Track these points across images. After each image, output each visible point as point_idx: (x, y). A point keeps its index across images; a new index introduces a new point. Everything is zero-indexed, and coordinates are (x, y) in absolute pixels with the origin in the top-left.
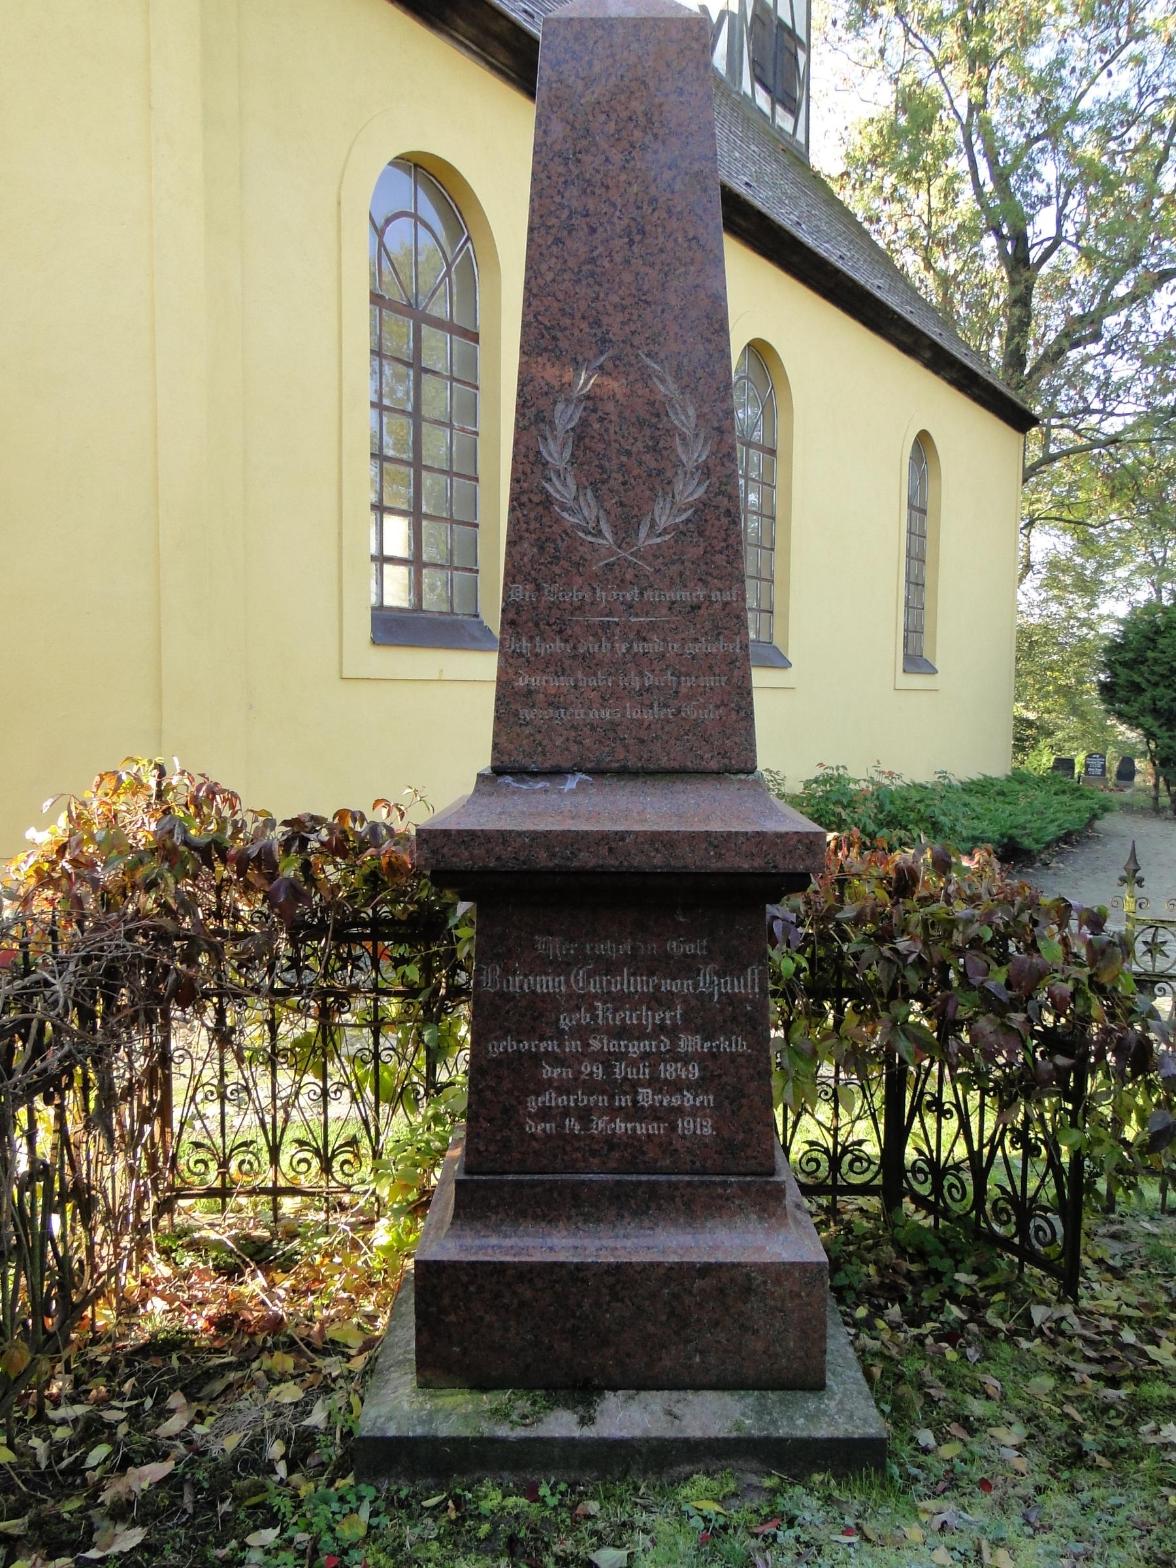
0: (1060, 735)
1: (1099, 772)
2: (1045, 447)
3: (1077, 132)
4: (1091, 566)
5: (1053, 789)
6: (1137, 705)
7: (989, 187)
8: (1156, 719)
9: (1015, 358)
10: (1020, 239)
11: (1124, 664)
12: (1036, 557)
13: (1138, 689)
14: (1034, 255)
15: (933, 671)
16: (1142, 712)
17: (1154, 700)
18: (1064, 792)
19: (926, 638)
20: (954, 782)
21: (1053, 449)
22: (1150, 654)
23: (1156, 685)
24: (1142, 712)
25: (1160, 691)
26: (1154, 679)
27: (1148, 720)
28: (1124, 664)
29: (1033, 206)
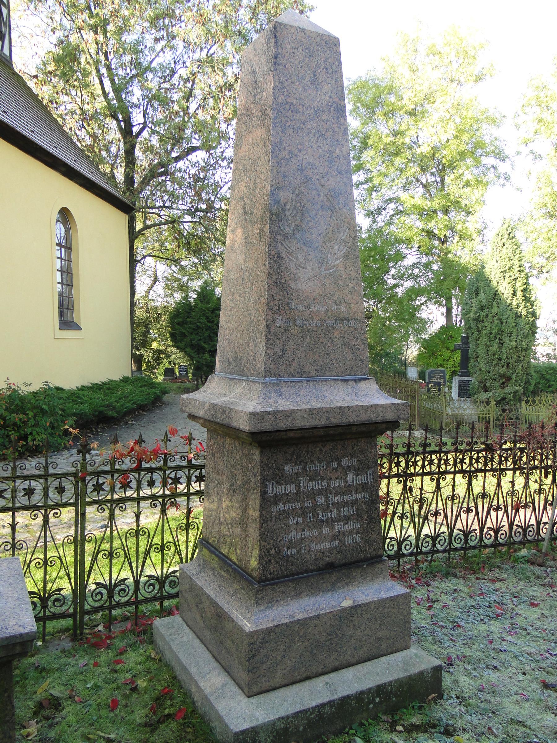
0: (173, 357)
1: (185, 373)
2: (145, 222)
3: (150, 76)
4: (185, 279)
5: (140, 385)
6: (183, 343)
7: (111, 95)
8: (192, 349)
9: (129, 180)
10: (128, 121)
11: (178, 324)
12: (159, 275)
13: (183, 335)
14: (135, 130)
15: (79, 328)
16: (186, 346)
17: (191, 340)
18: (145, 386)
19: (75, 311)
20: (51, 386)
21: (148, 223)
22: (188, 319)
23: (192, 333)
24: (186, 346)
25: (193, 336)
26: (191, 331)
27: (188, 350)
28: (178, 324)
29: (132, 107)
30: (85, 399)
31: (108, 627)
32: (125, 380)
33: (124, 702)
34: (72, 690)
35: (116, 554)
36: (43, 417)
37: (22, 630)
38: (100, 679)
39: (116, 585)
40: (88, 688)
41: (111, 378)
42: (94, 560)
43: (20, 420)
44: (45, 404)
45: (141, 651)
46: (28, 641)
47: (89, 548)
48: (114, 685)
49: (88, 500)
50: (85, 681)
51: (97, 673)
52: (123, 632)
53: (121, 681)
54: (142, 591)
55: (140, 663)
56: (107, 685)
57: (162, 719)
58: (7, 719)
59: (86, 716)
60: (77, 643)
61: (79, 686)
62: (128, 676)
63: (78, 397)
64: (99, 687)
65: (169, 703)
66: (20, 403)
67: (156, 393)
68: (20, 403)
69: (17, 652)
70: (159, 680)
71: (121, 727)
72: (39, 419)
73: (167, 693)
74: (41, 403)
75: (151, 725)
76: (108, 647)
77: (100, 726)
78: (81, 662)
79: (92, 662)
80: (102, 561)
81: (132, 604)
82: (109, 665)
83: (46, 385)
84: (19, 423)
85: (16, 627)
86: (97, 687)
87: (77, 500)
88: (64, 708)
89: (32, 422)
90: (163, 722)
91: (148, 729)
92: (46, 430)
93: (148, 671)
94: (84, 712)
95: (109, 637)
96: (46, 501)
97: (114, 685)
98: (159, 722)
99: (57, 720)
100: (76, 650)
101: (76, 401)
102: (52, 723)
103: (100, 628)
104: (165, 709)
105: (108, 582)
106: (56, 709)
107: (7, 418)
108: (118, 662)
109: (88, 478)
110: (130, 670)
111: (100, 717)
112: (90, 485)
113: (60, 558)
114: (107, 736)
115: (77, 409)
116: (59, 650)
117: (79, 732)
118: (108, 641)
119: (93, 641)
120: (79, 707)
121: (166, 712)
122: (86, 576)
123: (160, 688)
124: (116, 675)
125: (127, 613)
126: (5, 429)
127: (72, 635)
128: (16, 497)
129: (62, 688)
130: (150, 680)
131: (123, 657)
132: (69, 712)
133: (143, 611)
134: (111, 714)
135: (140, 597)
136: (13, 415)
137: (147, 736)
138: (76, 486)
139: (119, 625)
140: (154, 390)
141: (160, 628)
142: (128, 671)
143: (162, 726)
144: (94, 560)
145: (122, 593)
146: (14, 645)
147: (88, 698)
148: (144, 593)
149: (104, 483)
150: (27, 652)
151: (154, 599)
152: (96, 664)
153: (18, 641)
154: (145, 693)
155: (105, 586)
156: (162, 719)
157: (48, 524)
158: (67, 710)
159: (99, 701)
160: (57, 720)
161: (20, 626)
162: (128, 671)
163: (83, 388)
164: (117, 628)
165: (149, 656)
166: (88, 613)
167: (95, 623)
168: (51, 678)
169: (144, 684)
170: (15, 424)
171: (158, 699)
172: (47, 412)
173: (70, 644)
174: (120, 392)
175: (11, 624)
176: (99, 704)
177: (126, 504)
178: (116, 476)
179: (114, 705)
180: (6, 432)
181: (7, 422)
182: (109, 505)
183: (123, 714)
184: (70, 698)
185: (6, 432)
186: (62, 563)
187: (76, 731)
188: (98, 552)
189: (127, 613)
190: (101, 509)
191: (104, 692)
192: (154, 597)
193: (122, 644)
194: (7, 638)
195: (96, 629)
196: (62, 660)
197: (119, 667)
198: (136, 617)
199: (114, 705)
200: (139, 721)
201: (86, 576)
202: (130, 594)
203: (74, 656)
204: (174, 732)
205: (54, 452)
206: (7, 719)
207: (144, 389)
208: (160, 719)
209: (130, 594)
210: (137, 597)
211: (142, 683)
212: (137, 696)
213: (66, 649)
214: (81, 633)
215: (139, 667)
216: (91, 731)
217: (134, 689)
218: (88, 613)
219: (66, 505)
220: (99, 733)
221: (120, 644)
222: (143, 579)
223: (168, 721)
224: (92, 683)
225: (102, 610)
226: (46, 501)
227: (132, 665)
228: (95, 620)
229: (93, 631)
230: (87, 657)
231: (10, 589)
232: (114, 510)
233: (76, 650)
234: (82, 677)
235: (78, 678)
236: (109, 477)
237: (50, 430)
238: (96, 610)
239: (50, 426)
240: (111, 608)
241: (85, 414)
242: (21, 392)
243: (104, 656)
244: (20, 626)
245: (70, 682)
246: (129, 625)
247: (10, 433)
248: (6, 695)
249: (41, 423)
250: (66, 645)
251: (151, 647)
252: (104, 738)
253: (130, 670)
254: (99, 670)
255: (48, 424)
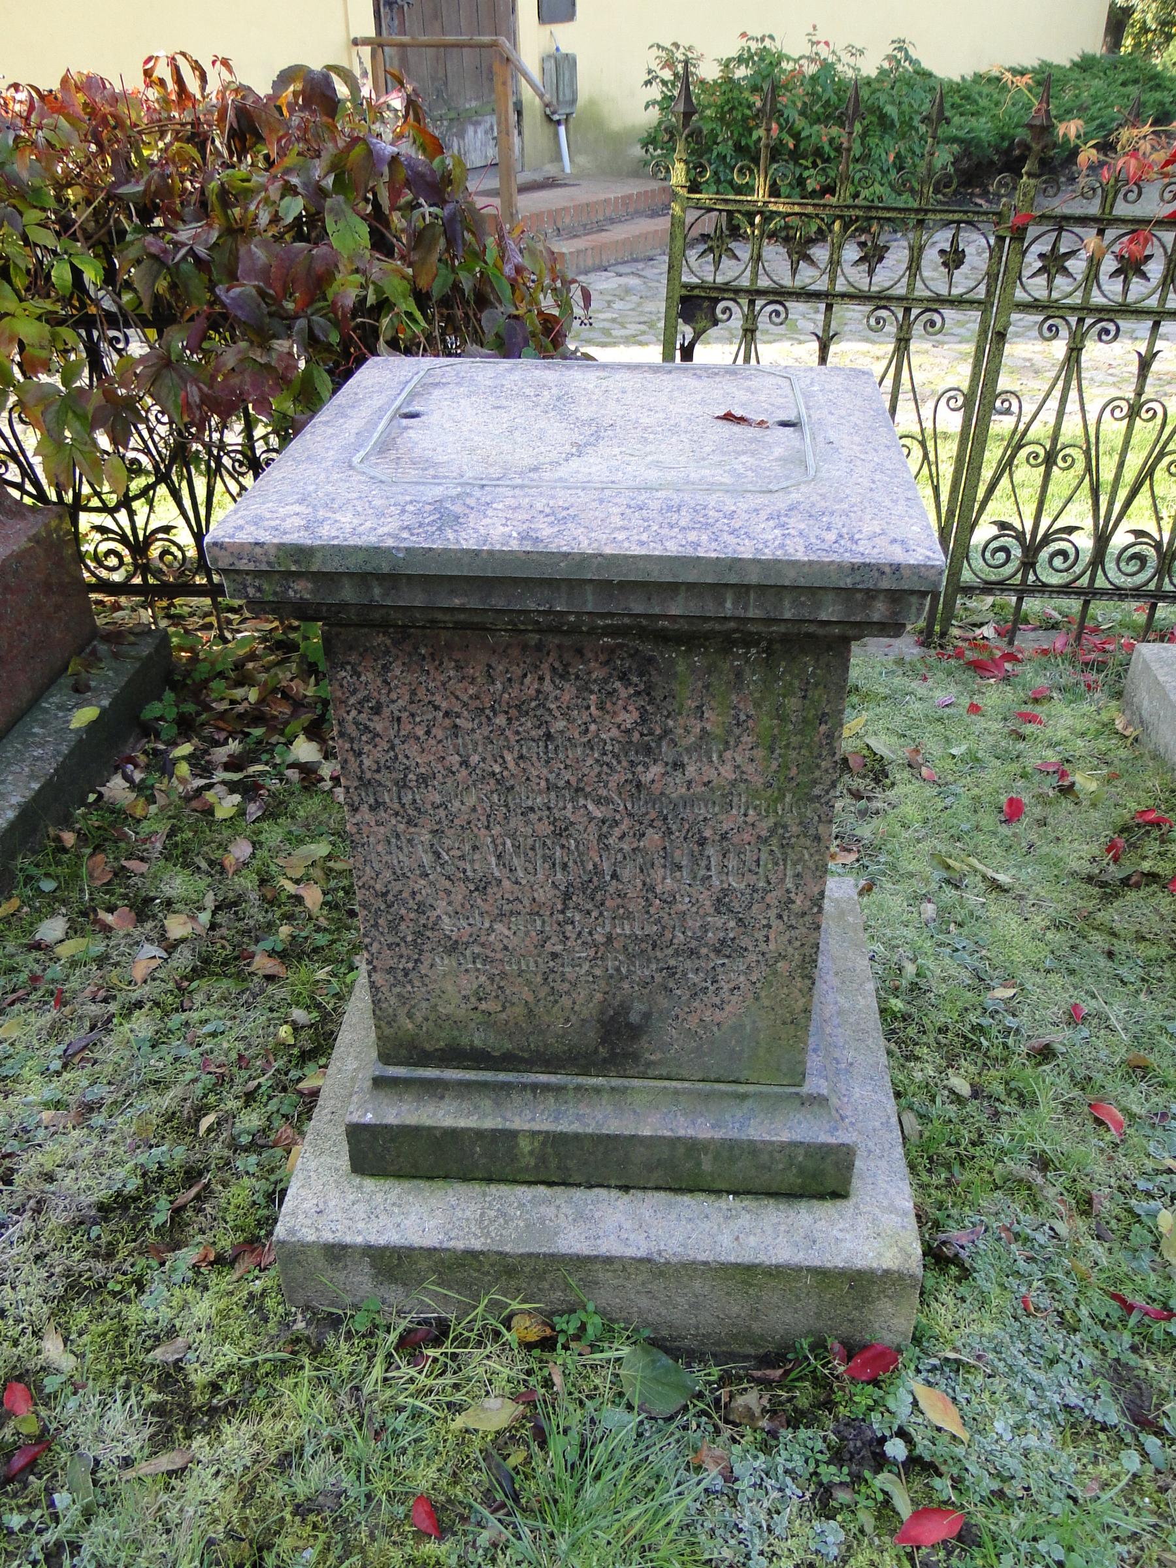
5: (1122, 78)
18: (1136, 81)
30: (983, 102)
31: (1009, 633)
32: (1086, 65)
33: (1038, 811)
34: (917, 751)
35: (1064, 459)
36: (881, 138)
37: (898, 555)
38: (982, 745)
39: (1047, 540)
40: (954, 757)
41: (1049, 59)
42: (1007, 465)
43: (831, 141)
44: (893, 103)
45: (1085, 708)
46: (912, 592)
47: (1001, 425)
48: (1014, 767)
49: (1020, 295)
50: (947, 740)
51: (976, 729)
52: (1045, 652)
53: (1031, 762)
54: (1110, 565)
55: (1083, 735)
56: (998, 763)
57: (1134, 880)
58: (817, 791)
59: (945, 815)
60: (933, 652)
61: (933, 747)
62: (1052, 756)
63: (967, 98)
64: (977, 760)
65: (1156, 847)
66: (834, 99)
67: (1162, 104)
68: (834, 99)
69: (876, 617)
70: (1130, 787)
71: (1026, 865)
72: (872, 141)
73: (1157, 824)
74: (883, 98)
75: (1103, 885)
76: (1007, 679)
77: (976, 846)
78: (940, 696)
79: (965, 701)
80: (1027, 475)
81: (1079, 593)
82: (1005, 719)
83: (900, 49)
84: (827, 148)
85: (881, 542)
86: (974, 760)
87: (989, 293)
88: (893, 784)
89: (857, 150)
90: (1137, 886)
91: (1096, 890)
92: (885, 173)
93: (1103, 759)
94: (940, 806)
95: (1010, 657)
96: (911, 286)
97: (1014, 767)
98: (1125, 882)
99: (877, 805)
100: (930, 668)
101: (960, 106)
102: (867, 809)
103: (988, 631)
104: (1144, 858)
105: (1028, 528)
106: (877, 781)
107: (803, 135)
108: (1030, 719)
109: (1032, 231)
110: (1058, 744)
111: (977, 828)
112: (1036, 249)
113: (923, 444)
114: (990, 873)
115: (960, 127)
116: (891, 658)
117: (925, 846)
118: (1008, 666)
119: (970, 655)
120: (933, 791)
121: (1146, 866)
122: (977, 506)
123: (1133, 806)
124: (1021, 746)
125: (1055, 614)
126: (796, 163)
127: (921, 632)
128: (839, 263)
129: (894, 739)
130: (1110, 780)
131: (1038, 710)
132: (906, 796)
133: (1094, 618)
134: (1004, 830)
135: (1100, 582)
136: (816, 127)
137: (1090, 905)
138: (995, 253)
139: (1032, 635)
140: (1158, 95)
141: (1154, 666)
142: (1052, 745)
143: (1132, 896)
144: (1007, 465)
145: (1058, 562)
146: (871, 594)
147: (950, 778)
148: (1113, 575)
149: (1072, 254)
150: (904, 625)
151: (1137, 593)
152: (974, 709)
153: (885, 584)
154: (1094, 805)
155: (1020, 536)
156: (1134, 880)
157: (907, 348)
158: (899, 790)
159: (976, 791)
160: (877, 805)
161: (894, 541)
162: (1052, 745)
163: (978, 77)
164: (1027, 642)
165: (1109, 725)
166: (968, 590)
167: (976, 619)
168: (871, 713)
169: (1093, 786)
170: (818, 152)
171: (1125, 829)
172: (893, 124)
173: (917, 650)
174: (1068, 96)
175: (867, 529)
176: (976, 799)
177: (1120, 322)
178: (1111, 233)
179: (1013, 811)
180: (798, 171)
181: (802, 146)
182: (1073, 320)
183: (1033, 837)
184: (910, 766)
185: (798, 171)
186: (926, 456)
187: (918, 841)
188: (1020, 447)
189: (1055, 614)
190: (1050, 329)
191: (989, 775)
192: (1137, 589)
193: (1040, 682)
194: (854, 568)
195: (978, 631)
196: (896, 681)
197: (1028, 729)
198: (1082, 627)
199: (1013, 811)
200: (1075, 865)
201: (977, 506)
202: (1078, 569)
203: (925, 679)
204: (1162, 919)
205: (895, 231)
206: (817, 791)
207: (1133, 90)
208: (1129, 878)
209: (1078, 569)
210: (1093, 579)
211: (1085, 781)
212: (1071, 807)
213: (908, 659)
214: (943, 634)
215: (1080, 742)
216: (955, 852)
217: (1067, 790)
218: (968, 590)
219: (958, 302)
220: (973, 861)
221: (1033, 677)
222: (1120, 539)
223: (1150, 889)
224: (963, 748)
225: (1003, 590)
226: (911, 286)
227: (1062, 734)
228: (973, 611)
229: (970, 635)
230: (953, 689)
231: (857, 439)
232: (1084, 336)
233: (930, 668)
234: (939, 728)
235: (930, 728)
236: (1090, 235)
237: (893, 175)
238: (988, 588)
239: (894, 163)
240: (1023, 591)
241: (979, 145)
242: (839, 67)
243: (994, 695)
244: (894, 541)
245: (911, 733)
246: (1058, 640)
247: (806, 174)
248: (823, 728)
249: (875, 153)
250: (905, 650)
251: (1114, 703)
252: (984, 877)
253: (1058, 744)
254: (981, 723)
255: (891, 159)
